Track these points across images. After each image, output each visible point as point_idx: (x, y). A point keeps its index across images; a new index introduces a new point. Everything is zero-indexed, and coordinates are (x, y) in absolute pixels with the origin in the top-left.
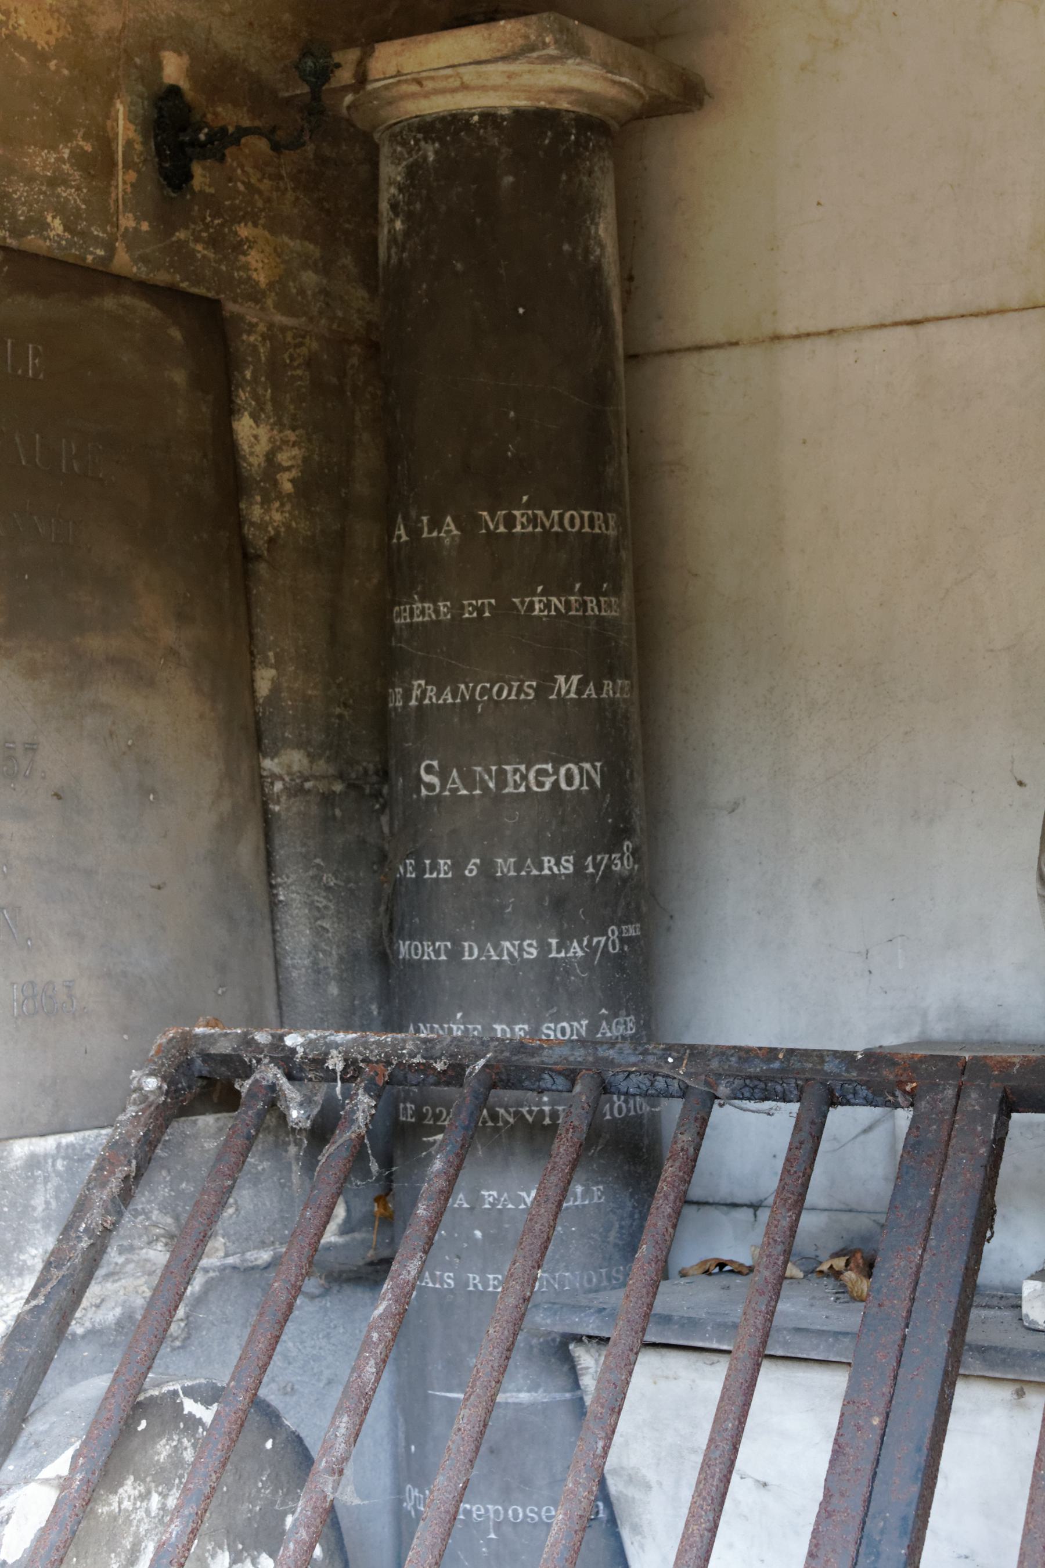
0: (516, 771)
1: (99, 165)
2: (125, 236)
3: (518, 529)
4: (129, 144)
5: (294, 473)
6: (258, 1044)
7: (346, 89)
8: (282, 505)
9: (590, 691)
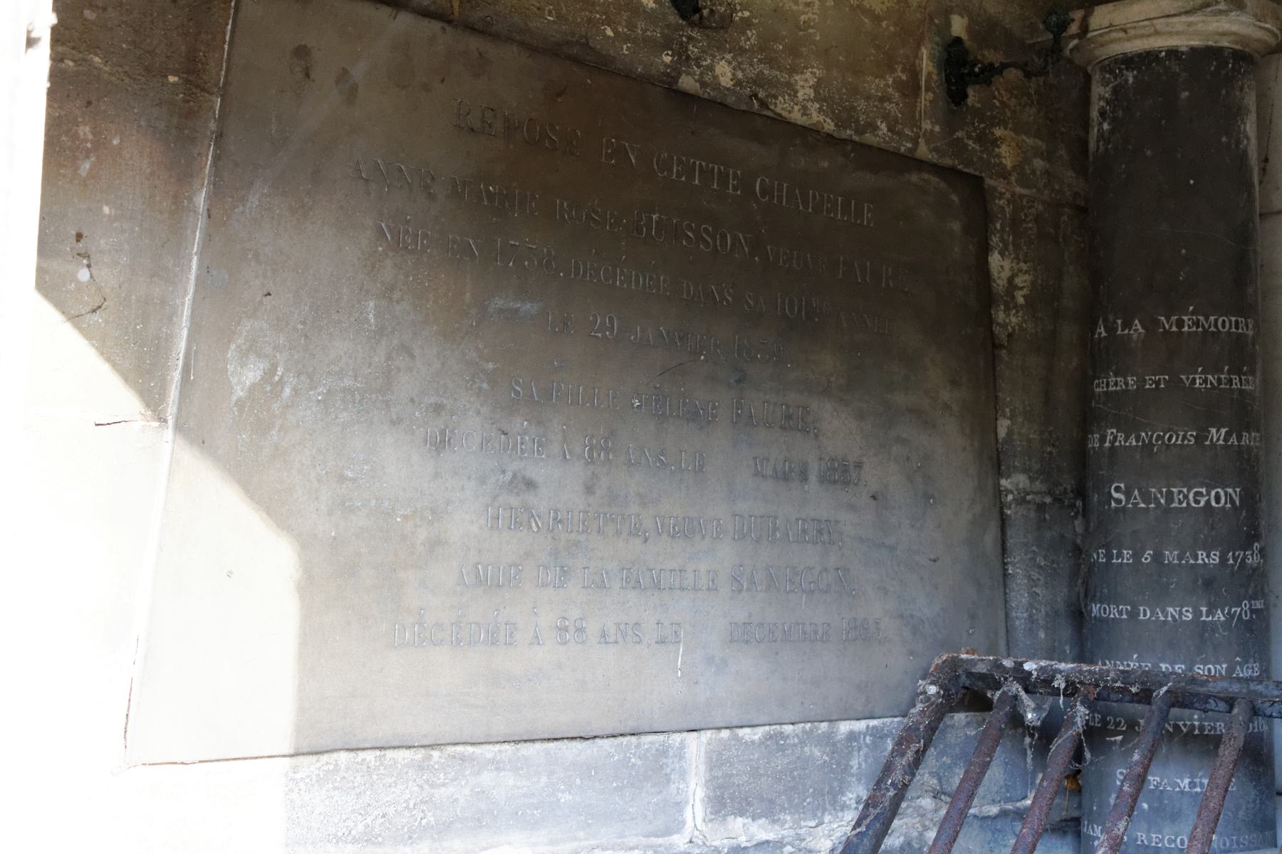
0: (1180, 492)
1: (911, 89)
2: (925, 136)
3: (1186, 328)
4: (929, 74)
5: (1025, 292)
6: (1004, 667)
7: (1072, 37)
9: (1233, 440)
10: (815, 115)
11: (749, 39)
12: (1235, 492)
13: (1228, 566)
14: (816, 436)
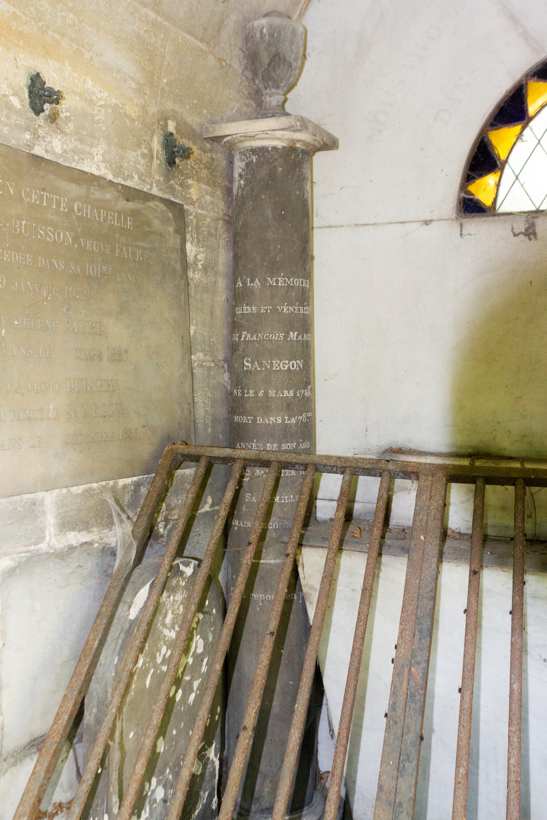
3: (280, 284)
4: (158, 151)
5: (202, 262)
8: (199, 272)
10: (103, 169)
11: (69, 128)
12: (300, 363)
13: (297, 397)
14: (106, 337)
